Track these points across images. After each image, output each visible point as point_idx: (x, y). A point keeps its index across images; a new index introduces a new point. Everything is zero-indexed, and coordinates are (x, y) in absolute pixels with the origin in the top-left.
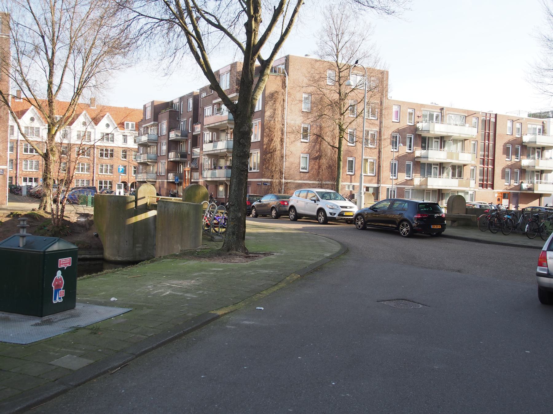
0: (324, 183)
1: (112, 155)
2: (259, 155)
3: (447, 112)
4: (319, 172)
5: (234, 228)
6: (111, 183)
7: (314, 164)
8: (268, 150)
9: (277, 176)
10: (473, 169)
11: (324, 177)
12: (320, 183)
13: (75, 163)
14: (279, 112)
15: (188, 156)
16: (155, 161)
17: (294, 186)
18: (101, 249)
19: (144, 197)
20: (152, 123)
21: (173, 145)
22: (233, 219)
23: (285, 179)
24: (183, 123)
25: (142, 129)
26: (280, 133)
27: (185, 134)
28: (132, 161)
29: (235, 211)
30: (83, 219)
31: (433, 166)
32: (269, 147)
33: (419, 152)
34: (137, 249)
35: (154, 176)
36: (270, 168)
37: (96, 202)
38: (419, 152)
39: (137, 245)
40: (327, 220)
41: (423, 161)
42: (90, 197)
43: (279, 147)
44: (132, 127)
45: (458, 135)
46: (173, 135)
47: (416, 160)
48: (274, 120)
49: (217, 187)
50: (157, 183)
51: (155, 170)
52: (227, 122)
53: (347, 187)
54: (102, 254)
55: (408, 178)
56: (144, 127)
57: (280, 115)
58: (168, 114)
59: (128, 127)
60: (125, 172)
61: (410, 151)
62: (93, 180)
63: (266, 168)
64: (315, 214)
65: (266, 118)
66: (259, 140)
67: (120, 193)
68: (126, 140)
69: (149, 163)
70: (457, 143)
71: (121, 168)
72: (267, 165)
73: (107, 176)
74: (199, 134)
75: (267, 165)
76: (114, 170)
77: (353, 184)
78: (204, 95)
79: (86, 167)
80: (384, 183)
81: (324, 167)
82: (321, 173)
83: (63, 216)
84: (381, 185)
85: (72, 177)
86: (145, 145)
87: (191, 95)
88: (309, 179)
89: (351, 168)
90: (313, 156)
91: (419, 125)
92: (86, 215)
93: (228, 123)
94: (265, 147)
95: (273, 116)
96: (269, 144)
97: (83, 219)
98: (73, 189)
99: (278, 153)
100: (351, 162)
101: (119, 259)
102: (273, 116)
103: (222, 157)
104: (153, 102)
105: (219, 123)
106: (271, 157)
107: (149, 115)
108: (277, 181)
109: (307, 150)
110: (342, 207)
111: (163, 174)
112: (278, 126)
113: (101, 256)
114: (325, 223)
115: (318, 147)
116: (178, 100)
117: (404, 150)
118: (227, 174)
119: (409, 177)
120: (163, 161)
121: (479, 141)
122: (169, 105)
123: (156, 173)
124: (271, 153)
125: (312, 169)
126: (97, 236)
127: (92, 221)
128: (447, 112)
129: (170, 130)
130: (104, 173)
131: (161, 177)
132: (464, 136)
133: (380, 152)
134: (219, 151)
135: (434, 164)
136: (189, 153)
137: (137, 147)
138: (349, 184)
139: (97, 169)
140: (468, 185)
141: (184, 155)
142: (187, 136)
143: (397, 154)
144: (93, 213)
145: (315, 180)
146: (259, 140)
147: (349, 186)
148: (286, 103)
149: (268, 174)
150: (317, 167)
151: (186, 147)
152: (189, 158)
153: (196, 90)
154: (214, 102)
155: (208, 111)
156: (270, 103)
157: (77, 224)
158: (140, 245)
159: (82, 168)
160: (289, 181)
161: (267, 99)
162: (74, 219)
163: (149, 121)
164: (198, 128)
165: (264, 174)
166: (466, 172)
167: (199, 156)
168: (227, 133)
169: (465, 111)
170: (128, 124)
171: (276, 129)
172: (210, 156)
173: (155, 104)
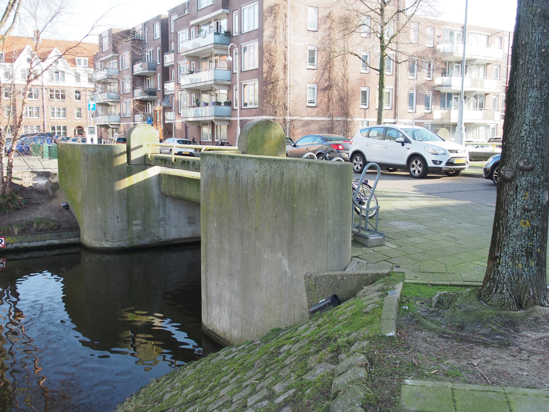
0: (335, 119)
1: (63, 97)
2: (257, 86)
3: (470, 31)
4: (329, 107)
5: (530, 239)
6: (65, 128)
7: (323, 96)
8: (268, 79)
9: (280, 111)
10: (495, 99)
11: (335, 112)
12: (331, 119)
13: (24, 94)
14: (280, 31)
15: (157, 93)
16: (118, 101)
17: (300, 125)
18: (75, 228)
19: (141, 146)
20: (111, 55)
21: (139, 80)
22: (526, 210)
23: (290, 115)
24: (149, 54)
25: (98, 65)
26: (282, 57)
27: (152, 68)
28: (88, 103)
29: (533, 185)
30: (42, 182)
31: (453, 96)
32: (270, 76)
33: (439, 80)
34: (134, 228)
35: (117, 118)
36: (272, 102)
37: (61, 154)
38: (439, 80)
39: (134, 222)
40: (427, 172)
41: (444, 90)
42: (46, 146)
43: (281, 76)
44: (85, 63)
45: (483, 58)
46: (138, 69)
47: (436, 89)
48: (275, 41)
49: (199, 128)
50: (122, 126)
51: (118, 112)
52: (212, 46)
53: (360, 123)
54: (79, 236)
55: (427, 111)
56: (101, 61)
57: (281, 35)
58: (129, 44)
59: (80, 64)
60: (79, 115)
61: (429, 79)
62: (44, 125)
63: (267, 103)
64: (404, 162)
65: (266, 38)
66: (257, 67)
67: (92, 140)
68: (77, 78)
69: (110, 104)
70: (479, 68)
71: (76, 111)
72: (268, 99)
73: (59, 121)
74: (172, 66)
75: (268, 99)
76: (67, 113)
77: (367, 119)
78: (175, 17)
79: (34, 111)
80: (401, 118)
81: (335, 100)
82: (331, 108)
83: (11, 178)
84: (399, 120)
85: (21, 117)
86: (105, 83)
87: (158, 18)
88: (318, 115)
89: (364, 101)
90: (322, 87)
91: (440, 47)
92: (46, 175)
93: (214, 48)
94: (265, 75)
95: (273, 36)
96: (270, 72)
97: (42, 182)
98: (23, 136)
99: (281, 83)
100: (364, 93)
101: (107, 246)
102: (273, 36)
103: (205, 92)
104: (110, 31)
105: (201, 49)
106: (274, 88)
107: (107, 46)
108: (282, 118)
109: (315, 78)
110: (450, 151)
111: (128, 116)
112: (280, 49)
113: (77, 239)
114: (423, 176)
115: (326, 74)
116: (141, 27)
117: (423, 76)
118: (215, 112)
119: (428, 109)
120: (128, 100)
121: (502, 66)
122: (127, 33)
123: (120, 114)
124: (273, 83)
125: (321, 103)
126: (67, 207)
127: (56, 184)
128: (470, 31)
129: (134, 61)
130: (56, 118)
131: (125, 119)
132: (488, 60)
133: (396, 80)
134: (203, 84)
135: (455, 94)
136: (159, 89)
137: (93, 86)
138: (363, 119)
139: (48, 111)
140: (492, 117)
141: (152, 93)
142: (155, 69)
143: (416, 82)
144: (56, 171)
145: (324, 115)
146: (257, 67)
147: (363, 122)
148: (288, 19)
149: (269, 109)
150: (326, 100)
151: (154, 83)
152: (159, 95)
153: (165, 14)
154: (192, 23)
155: (183, 35)
156: (270, 19)
157: (33, 189)
158: (139, 222)
159: (30, 112)
160: (294, 118)
161: (266, 14)
162: (27, 181)
163: (107, 53)
164: (169, 59)
165: (265, 110)
166: (489, 101)
167: (173, 92)
168: (211, 61)
169: (487, 30)
170: (79, 60)
171: (278, 53)
172: (190, 90)
173: (114, 32)
